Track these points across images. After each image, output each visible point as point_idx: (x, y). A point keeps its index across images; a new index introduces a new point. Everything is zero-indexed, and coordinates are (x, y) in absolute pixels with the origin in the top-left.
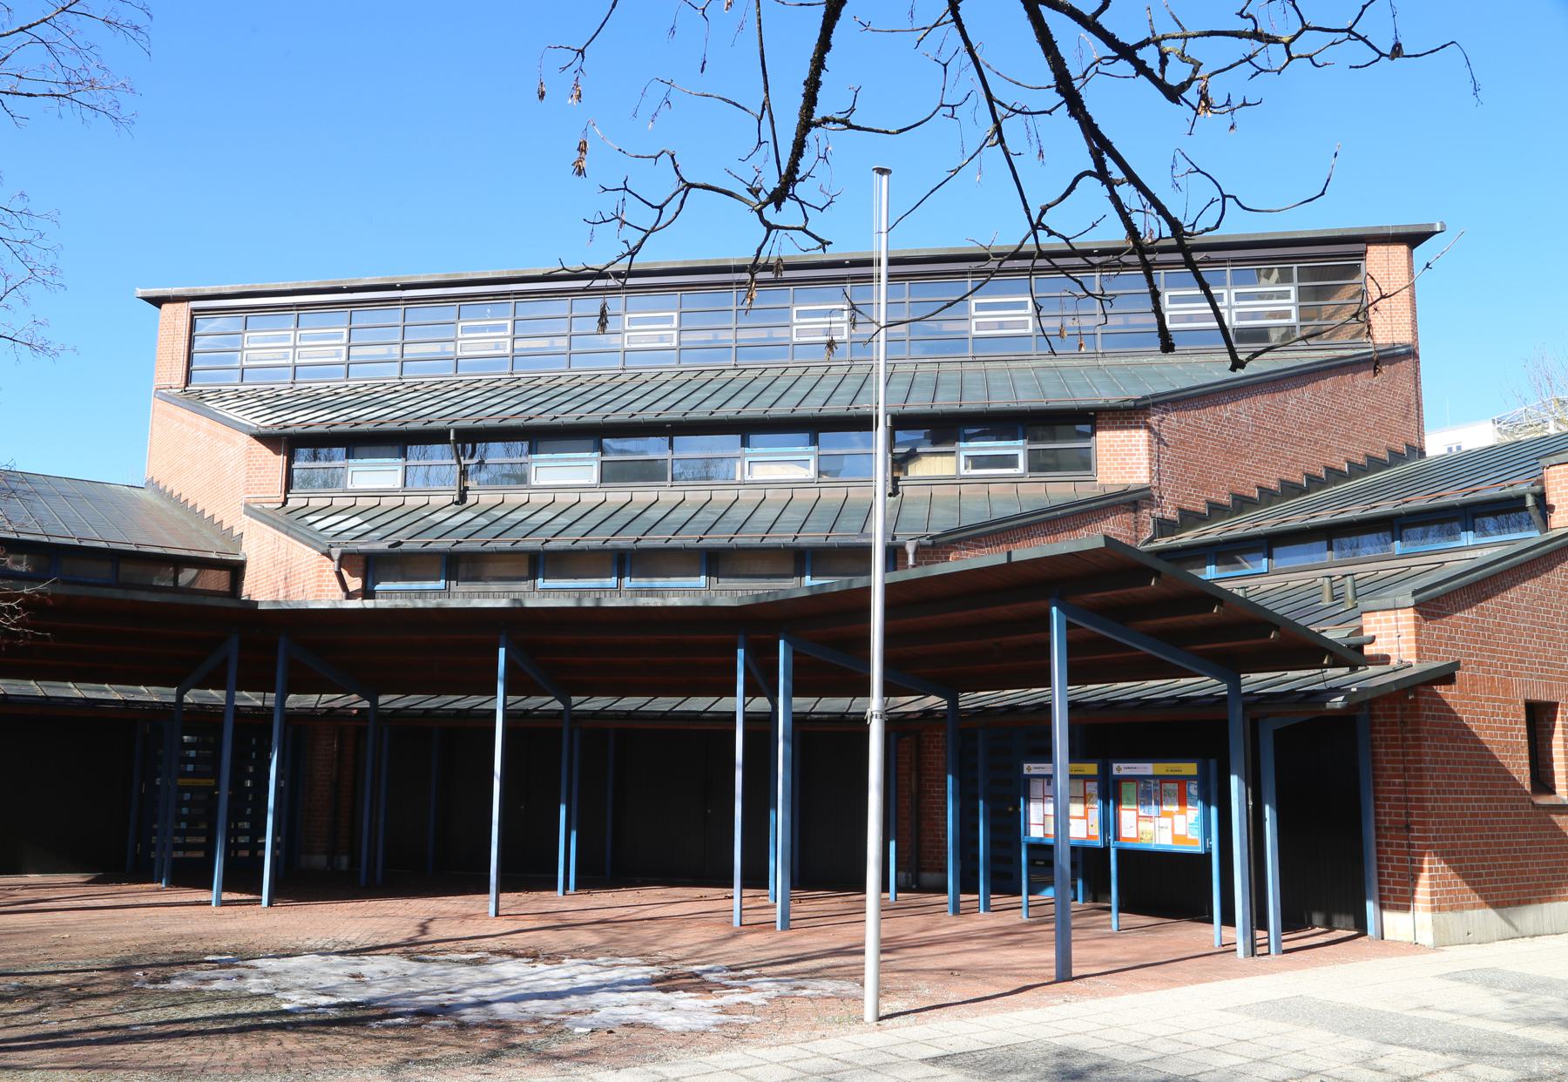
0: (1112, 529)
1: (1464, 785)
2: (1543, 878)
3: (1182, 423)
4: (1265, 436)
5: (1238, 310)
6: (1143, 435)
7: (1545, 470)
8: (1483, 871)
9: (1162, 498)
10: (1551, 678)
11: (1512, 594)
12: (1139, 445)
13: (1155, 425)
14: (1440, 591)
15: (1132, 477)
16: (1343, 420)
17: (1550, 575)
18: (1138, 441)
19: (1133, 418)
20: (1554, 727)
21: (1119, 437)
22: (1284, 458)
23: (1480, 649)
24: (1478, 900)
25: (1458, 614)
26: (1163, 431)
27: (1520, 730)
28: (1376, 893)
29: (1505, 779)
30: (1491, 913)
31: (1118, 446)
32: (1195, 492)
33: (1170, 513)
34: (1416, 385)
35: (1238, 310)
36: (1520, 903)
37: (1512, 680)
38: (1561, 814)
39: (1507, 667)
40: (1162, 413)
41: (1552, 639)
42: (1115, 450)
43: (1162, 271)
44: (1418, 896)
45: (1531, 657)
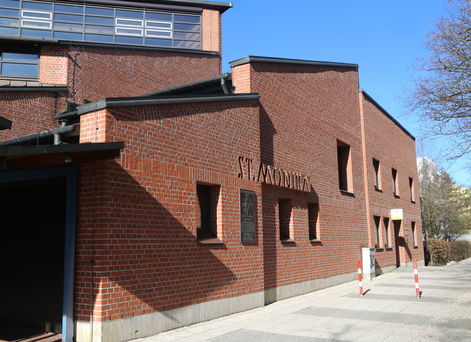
0: (38, 104)
1: (142, 232)
2: (202, 288)
3: (91, 59)
4: (141, 75)
5: (148, 30)
6: (65, 60)
7: (232, 68)
8: (154, 288)
9: (74, 93)
10: (217, 171)
11: (193, 118)
12: (63, 65)
13: (73, 56)
14: (131, 103)
15: (58, 81)
16: (183, 76)
17: (221, 114)
18: (63, 63)
19: (61, 51)
20: (218, 199)
21: (53, 60)
22: (151, 87)
23: (165, 146)
24: (147, 307)
25: (148, 122)
26: (78, 60)
27: (191, 199)
28: (71, 312)
29: (177, 228)
30: (158, 315)
31: (51, 64)
32: (97, 94)
33: (80, 102)
34: (220, 70)
35: (148, 30)
36: (182, 305)
37: (188, 168)
38: (218, 249)
39: (185, 160)
40: (78, 51)
41: (219, 149)
42: (49, 66)
43: (115, 9)
44: (95, 311)
45: (203, 156)
